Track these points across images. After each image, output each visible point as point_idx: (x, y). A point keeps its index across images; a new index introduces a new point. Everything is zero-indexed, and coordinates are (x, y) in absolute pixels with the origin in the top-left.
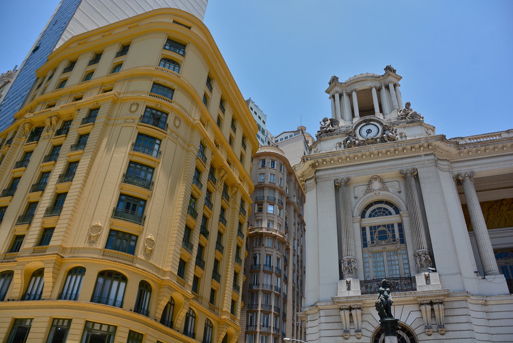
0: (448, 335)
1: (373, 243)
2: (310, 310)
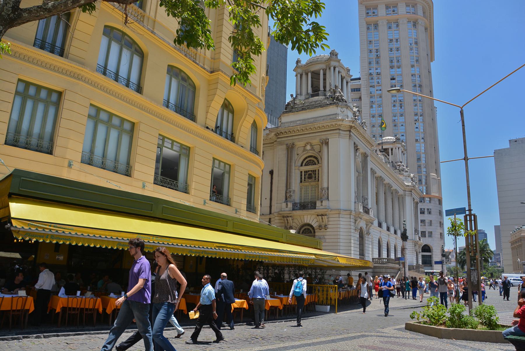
0: (328, 230)
1: (305, 180)
2: (343, 212)
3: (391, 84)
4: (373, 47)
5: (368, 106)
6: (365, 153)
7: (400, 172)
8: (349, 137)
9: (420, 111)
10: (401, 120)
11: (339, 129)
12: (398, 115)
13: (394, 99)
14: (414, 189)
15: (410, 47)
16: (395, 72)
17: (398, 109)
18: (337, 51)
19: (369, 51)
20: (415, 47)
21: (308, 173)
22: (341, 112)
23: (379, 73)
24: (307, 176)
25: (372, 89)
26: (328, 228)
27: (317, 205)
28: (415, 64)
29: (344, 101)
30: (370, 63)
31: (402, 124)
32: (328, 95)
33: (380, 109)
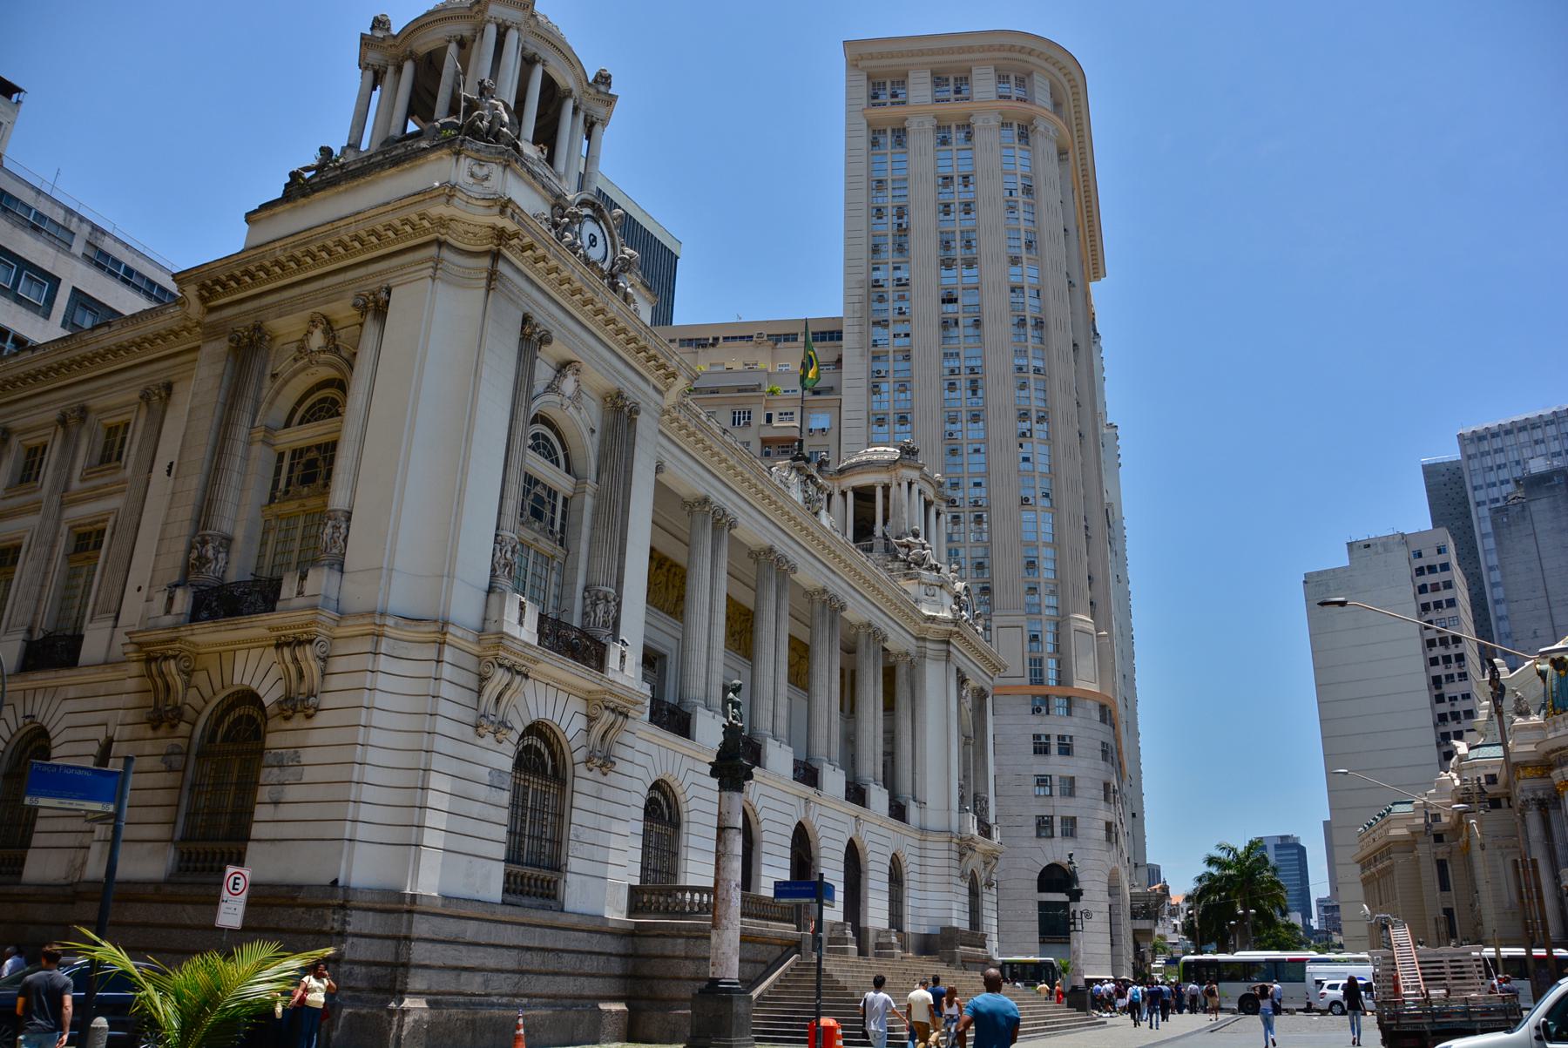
0: (321, 719)
2: (396, 626)
3: (944, 316)
4: (888, 201)
5: (864, 385)
6: (619, 394)
7: (909, 568)
8: (484, 283)
9: (1035, 405)
10: (969, 433)
11: (441, 244)
12: (964, 416)
13: (953, 363)
14: (958, 633)
15: (1007, 201)
16: (956, 278)
17: (964, 399)
19: (875, 211)
20: (1024, 203)
21: (304, 460)
22: (471, 180)
23: (904, 281)
24: (298, 470)
25: (879, 333)
26: (317, 709)
27: (284, 593)
28: (1023, 253)
29: (502, 139)
30: (876, 249)
31: (977, 446)
32: (441, 121)
33: (902, 396)
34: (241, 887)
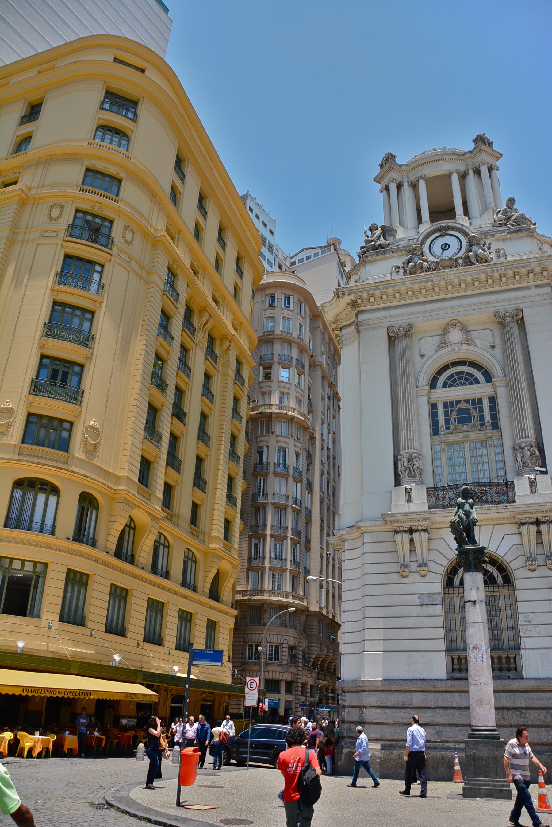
1: (448, 428)
18: (490, 137)
34: (254, 686)
